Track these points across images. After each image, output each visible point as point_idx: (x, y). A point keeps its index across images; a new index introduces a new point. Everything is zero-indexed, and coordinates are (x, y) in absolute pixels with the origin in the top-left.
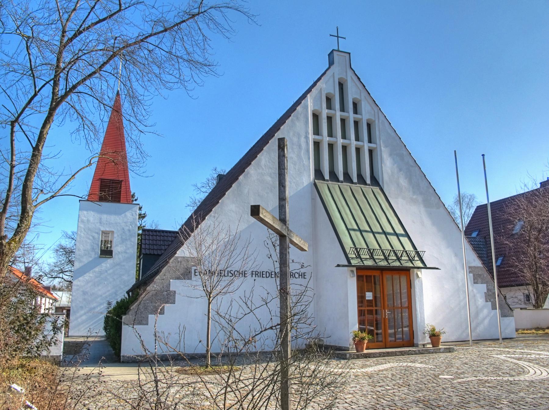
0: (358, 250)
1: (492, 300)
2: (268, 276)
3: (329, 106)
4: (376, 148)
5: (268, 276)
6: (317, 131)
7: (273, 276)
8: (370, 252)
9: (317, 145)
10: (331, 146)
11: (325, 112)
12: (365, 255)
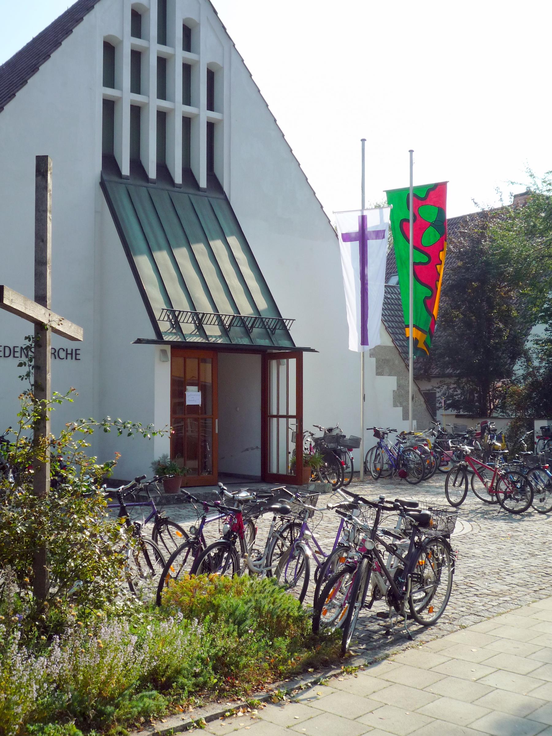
0: (177, 313)
1: (404, 404)
2: (7, 354)
3: (137, 29)
4: (222, 121)
5: (7, 354)
6: (110, 80)
7: (17, 355)
8: (198, 318)
9: (109, 107)
10: (136, 111)
11: (128, 43)
12: (188, 327)
